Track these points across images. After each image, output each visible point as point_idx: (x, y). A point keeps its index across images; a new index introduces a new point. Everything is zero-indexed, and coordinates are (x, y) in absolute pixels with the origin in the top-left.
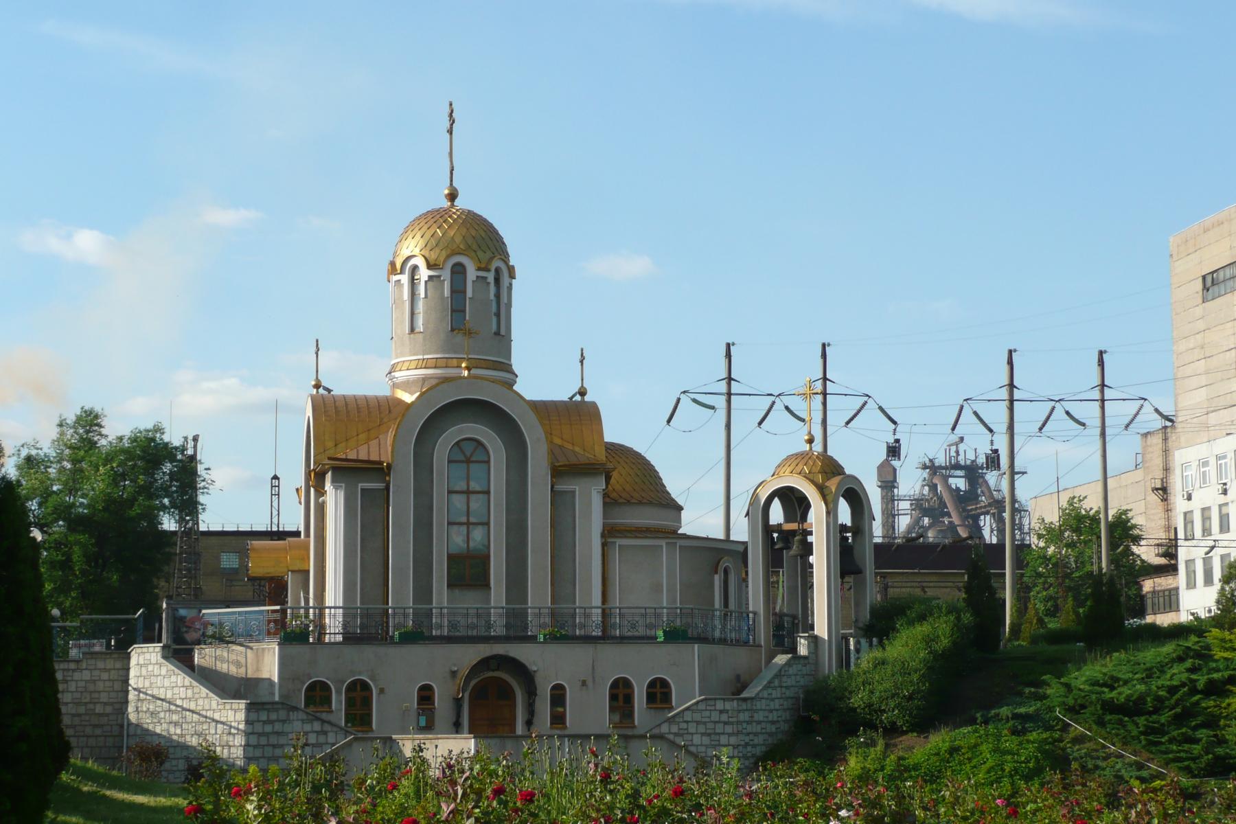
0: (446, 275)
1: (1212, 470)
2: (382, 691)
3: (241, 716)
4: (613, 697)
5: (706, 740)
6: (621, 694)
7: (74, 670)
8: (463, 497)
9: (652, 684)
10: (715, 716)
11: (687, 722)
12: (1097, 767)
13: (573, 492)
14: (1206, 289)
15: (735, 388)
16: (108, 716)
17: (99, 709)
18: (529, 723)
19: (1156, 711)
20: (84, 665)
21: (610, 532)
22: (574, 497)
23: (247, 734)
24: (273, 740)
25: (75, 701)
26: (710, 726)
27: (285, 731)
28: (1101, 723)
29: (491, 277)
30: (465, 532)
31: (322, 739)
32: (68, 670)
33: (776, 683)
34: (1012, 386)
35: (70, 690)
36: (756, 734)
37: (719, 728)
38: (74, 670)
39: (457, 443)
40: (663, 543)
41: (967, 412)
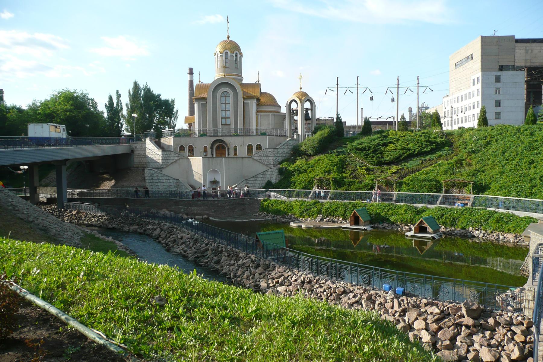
0: (224, 55)
1: (449, 103)
2: (196, 148)
3: (161, 153)
4: (248, 149)
5: (266, 158)
6: (250, 148)
8: (224, 105)
9: (257, 145)
10: (268, 153)
12: (352, 164)
14: (456, 66)
15: (339, 86)
18: (229, 154)
19: (368, 150)
21: (258, 112)
23: (162, 157)
24: (168, 158)
28: (355, 153)
29: (234, 55)
33: (286, 145)
34: (398, 84)
36: (279, 157)
37: (269, 155)
39: (223, 92)
40: (270, 114)
41: (388, 90)
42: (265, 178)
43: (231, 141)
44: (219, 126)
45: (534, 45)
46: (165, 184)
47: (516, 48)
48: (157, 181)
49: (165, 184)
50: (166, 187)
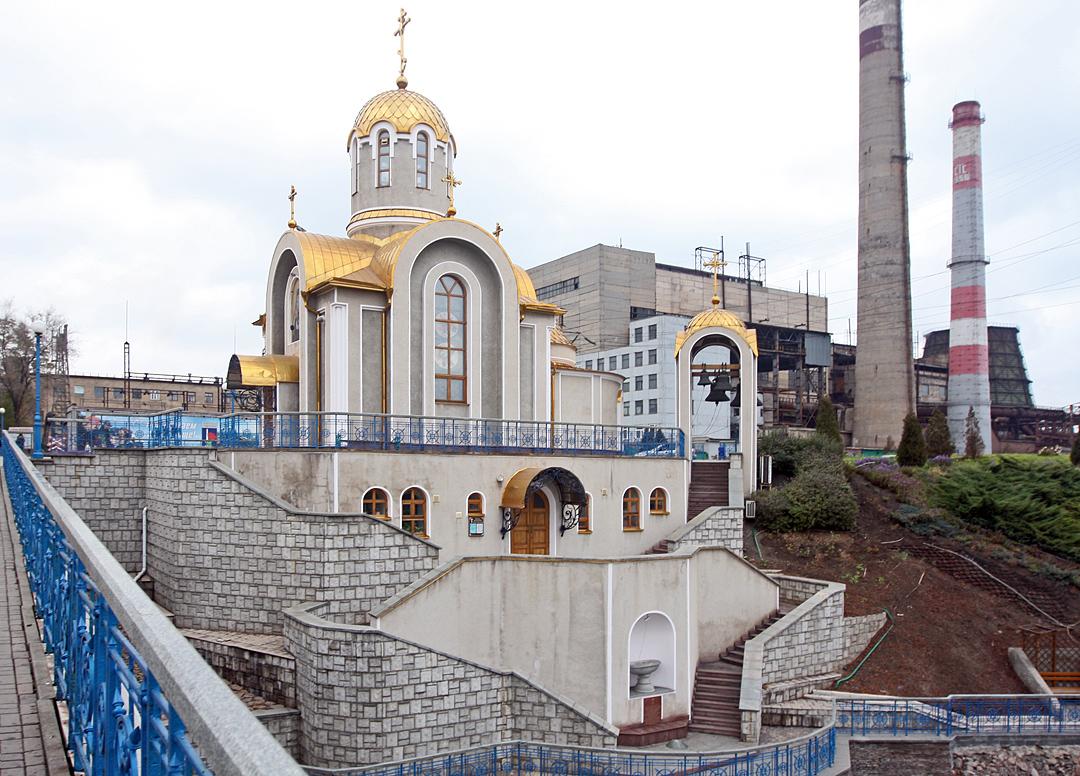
7: (87, 466)
11: (708, 529)
13: (532, 328)
16: (539, 702)
17: (114, 504)
20: (96, 461)
22: (532, 333)
24: (355, 555)
25: (89, 496)
26: (725, 532)
27: (366, 545)
30: (446, 355)
31: (404, 554)
32: (81, 465)
35: (83, 485)
38: (87, 466)
42: (816, 632)
43: (587, 472)
44: (429, 407)
45: (683, 276)
46: (448, 703)
47: (658, 278)
48: (409, 693)
49: (448, 703)
50: (454, 717)
